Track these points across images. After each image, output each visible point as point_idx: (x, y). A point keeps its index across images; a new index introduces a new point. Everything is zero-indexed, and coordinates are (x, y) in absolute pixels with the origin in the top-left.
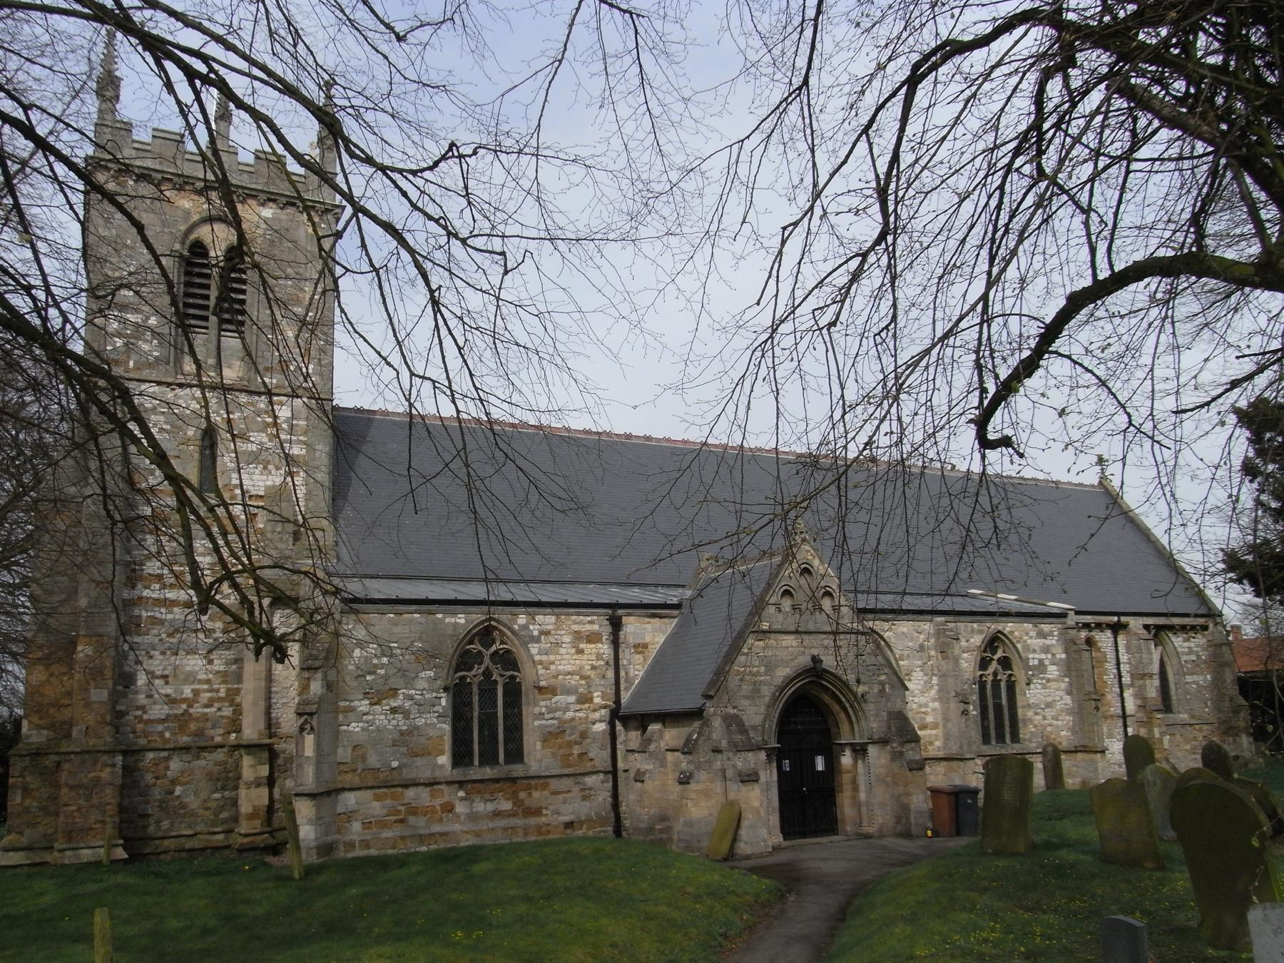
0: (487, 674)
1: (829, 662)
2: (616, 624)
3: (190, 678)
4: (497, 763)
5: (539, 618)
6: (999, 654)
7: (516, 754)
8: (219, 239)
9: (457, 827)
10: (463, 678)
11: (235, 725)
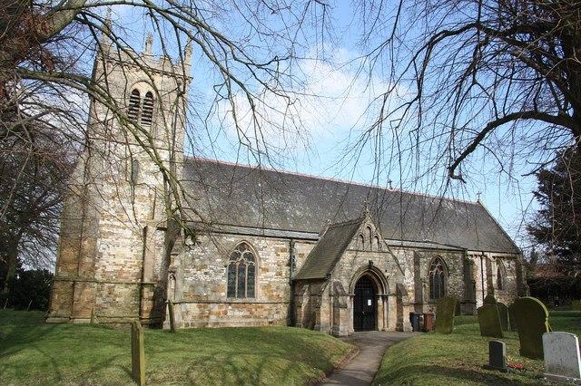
1: (376, 264)
2: (292, 246)
3: (123, 256)
7: (252, 294)
8: (144, 89)
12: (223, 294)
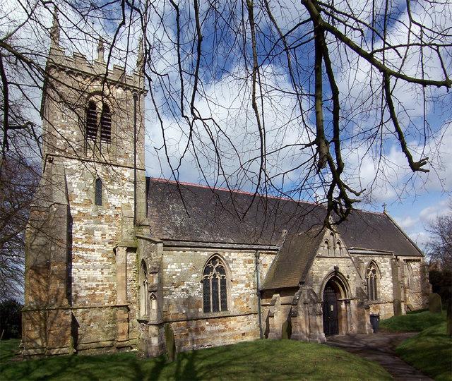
0: (215, 275)
1: (342, 269)
2: (257, 257)
3: (94, 280)
4: (218, 310)
5: (232, 254)
6: (372, 268)
7: (225, 308)
9: (206, 337)
10: (207, 277)
11: (113, 298)
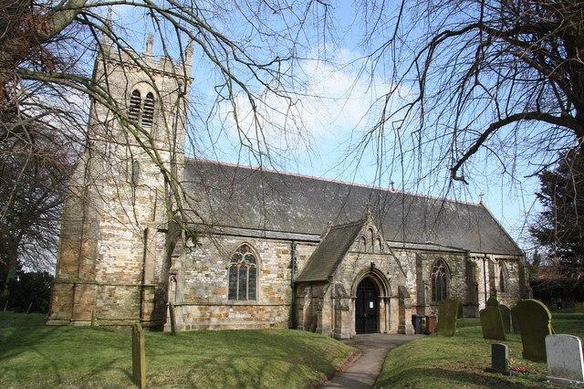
0: (439, 274)
1: (378, 266)
2: (293, 248)
3: (124, 258)
7: (253, 297)
8: (145, 90)
12: (224, 296)
